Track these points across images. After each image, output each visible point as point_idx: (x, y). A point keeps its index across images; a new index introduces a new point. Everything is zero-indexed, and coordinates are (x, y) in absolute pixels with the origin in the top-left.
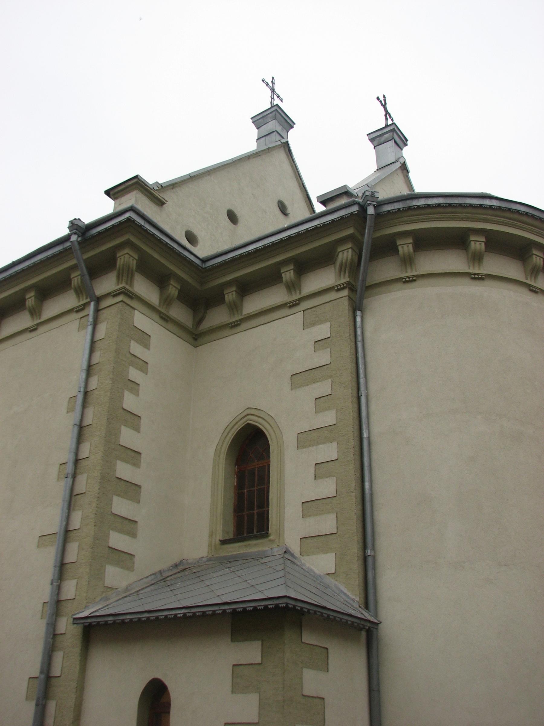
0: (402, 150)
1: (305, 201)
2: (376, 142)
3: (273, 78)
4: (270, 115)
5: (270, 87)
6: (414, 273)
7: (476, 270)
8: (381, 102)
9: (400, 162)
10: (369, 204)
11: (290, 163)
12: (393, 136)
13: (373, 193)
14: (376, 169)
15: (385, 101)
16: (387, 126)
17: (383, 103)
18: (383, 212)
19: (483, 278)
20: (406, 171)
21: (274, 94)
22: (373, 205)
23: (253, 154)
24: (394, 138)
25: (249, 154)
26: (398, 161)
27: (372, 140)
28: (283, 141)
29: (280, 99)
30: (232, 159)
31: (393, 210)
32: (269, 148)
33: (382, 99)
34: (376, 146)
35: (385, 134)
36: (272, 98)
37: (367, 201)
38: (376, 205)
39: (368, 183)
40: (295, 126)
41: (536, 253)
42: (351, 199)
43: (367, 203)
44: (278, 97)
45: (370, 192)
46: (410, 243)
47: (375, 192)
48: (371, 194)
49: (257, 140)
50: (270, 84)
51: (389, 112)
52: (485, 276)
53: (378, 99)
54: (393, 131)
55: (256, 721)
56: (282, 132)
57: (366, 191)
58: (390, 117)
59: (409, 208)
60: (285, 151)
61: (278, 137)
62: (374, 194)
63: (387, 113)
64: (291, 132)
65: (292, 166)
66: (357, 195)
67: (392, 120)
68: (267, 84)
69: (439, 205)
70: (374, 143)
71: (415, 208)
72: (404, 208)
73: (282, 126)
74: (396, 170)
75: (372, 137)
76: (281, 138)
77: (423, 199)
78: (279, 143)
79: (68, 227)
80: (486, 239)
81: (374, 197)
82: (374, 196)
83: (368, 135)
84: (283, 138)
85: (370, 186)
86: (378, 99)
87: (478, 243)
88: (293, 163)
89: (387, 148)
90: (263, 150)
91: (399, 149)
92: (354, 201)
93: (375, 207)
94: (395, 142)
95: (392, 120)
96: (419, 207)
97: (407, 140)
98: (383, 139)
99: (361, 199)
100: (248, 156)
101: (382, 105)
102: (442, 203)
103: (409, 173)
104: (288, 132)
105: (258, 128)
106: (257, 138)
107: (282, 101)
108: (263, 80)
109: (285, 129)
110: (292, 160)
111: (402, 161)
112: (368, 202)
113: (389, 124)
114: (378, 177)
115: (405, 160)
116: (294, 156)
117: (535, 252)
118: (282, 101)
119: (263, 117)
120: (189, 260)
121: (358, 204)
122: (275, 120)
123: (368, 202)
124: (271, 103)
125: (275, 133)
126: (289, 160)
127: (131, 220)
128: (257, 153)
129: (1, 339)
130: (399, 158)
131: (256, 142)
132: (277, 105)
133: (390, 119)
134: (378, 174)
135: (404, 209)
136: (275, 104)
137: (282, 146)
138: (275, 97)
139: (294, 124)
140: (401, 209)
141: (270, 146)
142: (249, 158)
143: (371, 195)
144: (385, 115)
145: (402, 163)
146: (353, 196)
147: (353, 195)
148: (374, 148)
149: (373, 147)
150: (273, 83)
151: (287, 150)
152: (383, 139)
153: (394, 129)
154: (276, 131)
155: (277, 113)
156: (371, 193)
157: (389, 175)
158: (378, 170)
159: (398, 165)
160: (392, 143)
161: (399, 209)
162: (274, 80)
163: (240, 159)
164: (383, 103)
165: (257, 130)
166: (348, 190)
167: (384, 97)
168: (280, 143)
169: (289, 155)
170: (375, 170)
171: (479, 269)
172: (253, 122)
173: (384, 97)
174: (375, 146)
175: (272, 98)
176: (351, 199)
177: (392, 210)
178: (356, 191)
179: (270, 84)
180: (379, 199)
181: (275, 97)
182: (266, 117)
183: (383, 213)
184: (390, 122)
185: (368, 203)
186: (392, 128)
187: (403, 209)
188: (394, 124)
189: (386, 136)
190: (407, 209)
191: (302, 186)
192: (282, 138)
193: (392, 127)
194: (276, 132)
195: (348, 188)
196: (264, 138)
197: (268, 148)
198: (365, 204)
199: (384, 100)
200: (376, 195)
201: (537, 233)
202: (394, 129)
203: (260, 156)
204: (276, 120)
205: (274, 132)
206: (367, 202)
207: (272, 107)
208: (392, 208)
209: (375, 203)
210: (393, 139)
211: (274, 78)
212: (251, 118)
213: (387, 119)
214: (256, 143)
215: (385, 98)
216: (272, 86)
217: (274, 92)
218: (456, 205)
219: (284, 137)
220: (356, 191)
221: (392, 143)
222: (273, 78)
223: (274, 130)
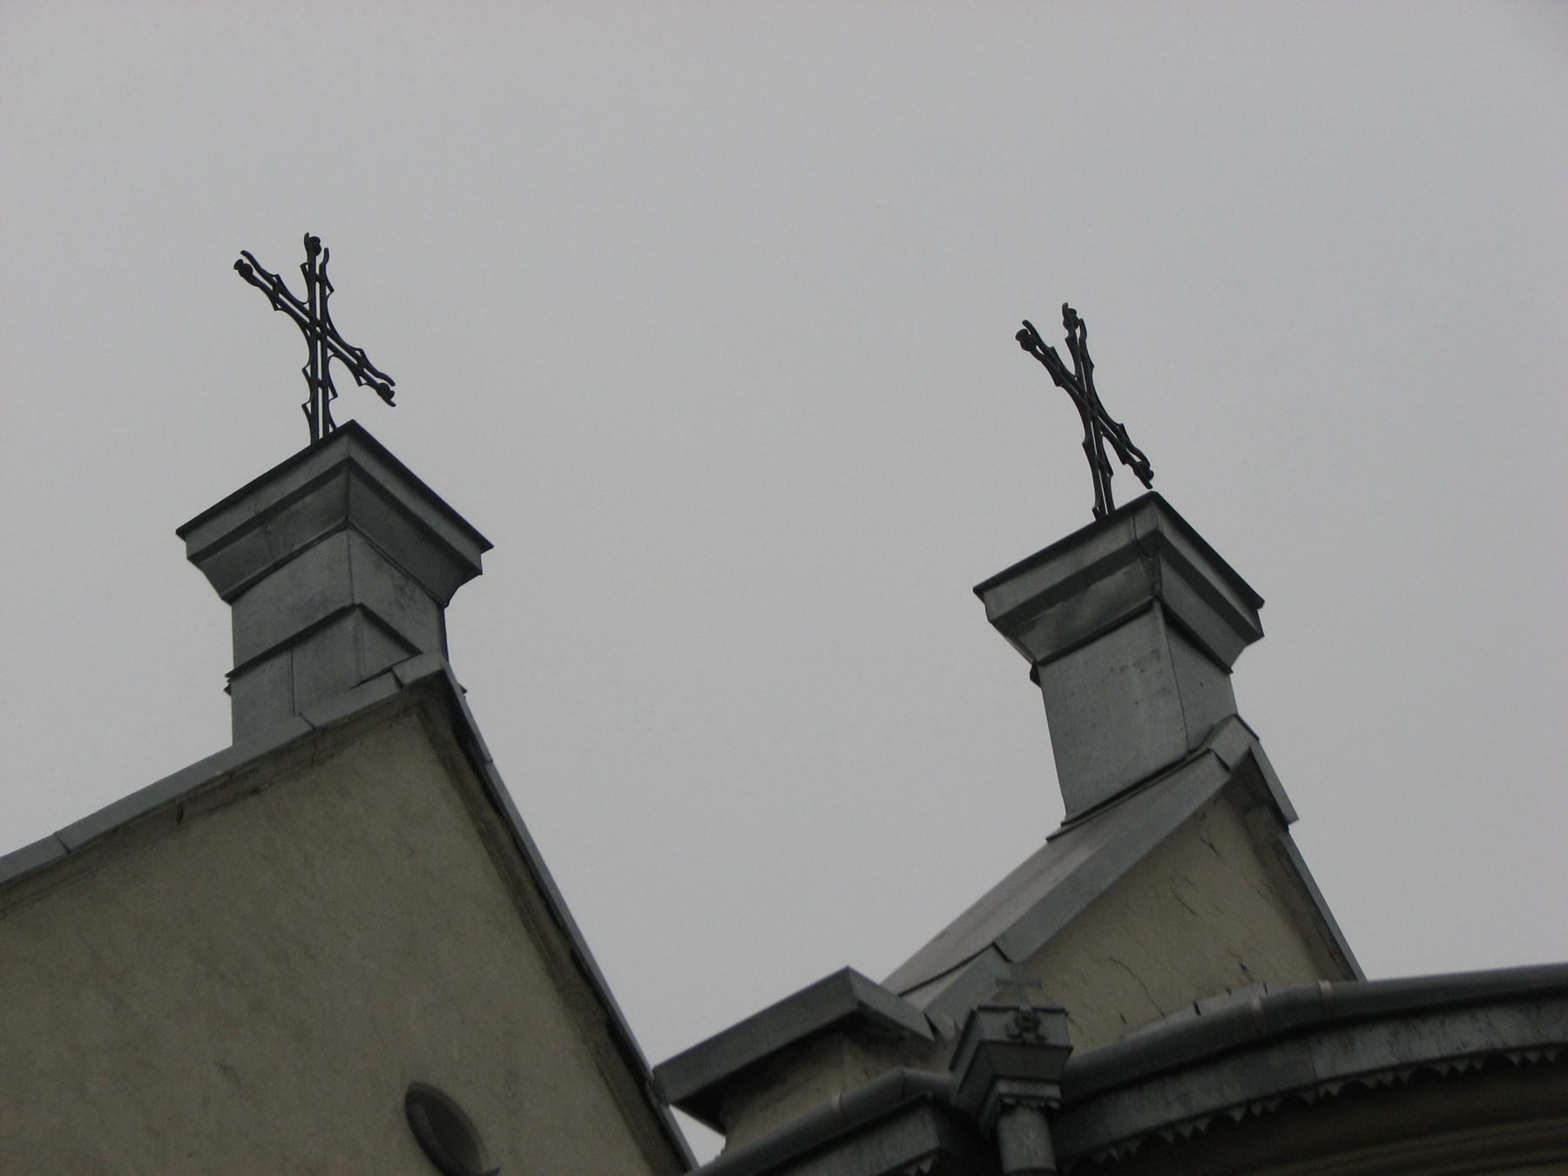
0: (1227, 671)
1: (601, 1073)
2: (1043, 634)
3: (312, 245)
4: (308, 499)
5: (299, 305)
8: (1049, 358)
9: (1217, 756)
10: (1009, 1101)
11: (476, 817)
12: (1153, 585)
13: (1029, 1022)
14: (1061, 815)
15: (1078, 347)
16: (1107, 517)
17: (1070, 365)
18: (1116, 1144)
20: (1266, 815)
21: (330, 353)
22: (1034, 1104)
23: (203, 785)
24: (1159, 597)
25: (181, 789)
26: (1208, 751)
27: (1011, 625)
28: (413, 671)
29: (371, 383)
30: (57, 835)
31: (1182, 1121)
32: (316, 735)
33: (1054, 335)
34: (1046, 662)
35: (1102, 576)
36: (320, 384)
37: (996, 1078)
38: (1055, 1105)
39: (1004, 937)
40: (486, 558)
42: (889, 1073)
43: (992, 1099)
44: (360, 367)
45: (1011, 1014)
47: (1041, 1015)
48: (1015, 1031)
49: (232, 676)
50: (298, 287)
51: (1117, 418)
53: (1029, 339)
54: (1150, 547)
56: (402, 607)
57: (983, 1009)
58: (1126, 449)
59: (1294, 1103)
60: (433, 740)
61: (377, 651)
62: (1037, 1024)
63: (1099, 427)
64: (465, 606)
65: (486, 837)
66: (927, 1033)
67: (1144, 472)
68: (276, 291)
69: (1495, 1063)
70: (1031, 639)
71: (1328, 1094)
72: (1248, 1103)
73: (398, 567)
74: (1200, 816)
75: (1007, 606)
76: (398, 654)
77: (1382, 1033)
78: (384, 690)
81: (1041, 1044)
82: (1041, 1038)
83: (980, 591)
84: (413, 651)
85: (1017, 955)
86: (1029, 339)
88: (490, 814)
89: (1122, 670)
90: (276, 755)
91: (1204, 669)
92: (905, 1085)
93: (1050, 1115)
94: (1175, 625)
95: (1144, 472)
96: (1355, 1088)
97: (1254, 602)
98: (1087, 608)
99: (952, 1067)
100: (172, 801)
101: (1060, 376)
102: (1513, 1043)
103: (1293, 829)
104: (441, 604)
105: (230, 598)
106: (231, 668)
107: (386, 393)
108: (246, 261)
109: (423, 587)
110: (483, 799)
111: (1229, 747)
113: (1119, 501)
114: (1073, 882)
115: (1257, 739)
116: (496, 762)
118: (386, 393)
119: (261, 519)
121: (936, 1103)
122: (341, 538)
123: (1002, 1087)
124: (312, 419)
125: (349, 624)
126: (464, 792)
128: (231, 776)
129: (13, 884)
130: (1212, 732)
131: (228, 690)
132: (353, 429)
133: (1128, 469)
134: (1080, 856)
135: (1257, 1110)
136: (340, 420)
137: (406, 709)
138: (339, 371)
139: (485, 545)
140: (1237, 1115)
141: (320, 719)
142: (180, 818)
143: (1020, 1036)
144: (1087, 446)
145: (1230, 762)
146: (901, 1039)
147: (906, 1034)
148: (1035, 677)
149: (1029, 667)
150: (316, 277)
151: (447, 733)
152: (1087, 608)
153: (1156, 536)
154: (361, 606)
155: (358, 487)
156: (1016, 1021)
157: (1150, 860)
158: (1069, 825)
159: (1206, 780)
160: (1147, 633)
161: (1219, 1118)
162: (319, 259)
163: (114, 831)
164: (1070, 365)
165: (227, 609)
166: (861, 1004)
167: (1071, 319)
168: (394, 690)
169: (463, 763)
170: (1054, 826)
172: (195, 558)
173: (1071, 319)
174: (1039, 658)
175: (313, 383)
176: (889, 1073)
177: (1170, 1125)
178: (921, 1001)
179: (298, 287)
180: (1074, 1055)
181: (339, 371)
182: (286, 513)
183: (1114, 1153)
184: (1126, 488)
185: (1001, 1096)
186: (1140, 534)
187: (1248, 1115)
188: (1154, 500)
189: (1108, 585)
190: (1272, 1107)
191: (572, 969)
192: (406, 656)
193: (1142, 526)
194: (358, 614)
195: (862, 994)
196: (281, 662)
197: (307, 735)
199: (1071, 341)
200: (1052, 1030)
202: (1156, 536)
203: (256, 791)
204: (351, 533)
205: (343, 613)
206: (992, 1085)
207: (317, 447)
208: (1176, 1113)
209: (1053, 1091)
210: (1157, 605)
211: (323, 245)
212: (183, 532)
213: (1101, 470)
214: (227, 700)
215: (1078, 331)
216: (312, 300)
217: (324, 342)
219: (418, 643)
220: (921, 1001)
221: (1147, 633)
222: (312, 245)
223: (347, 603)
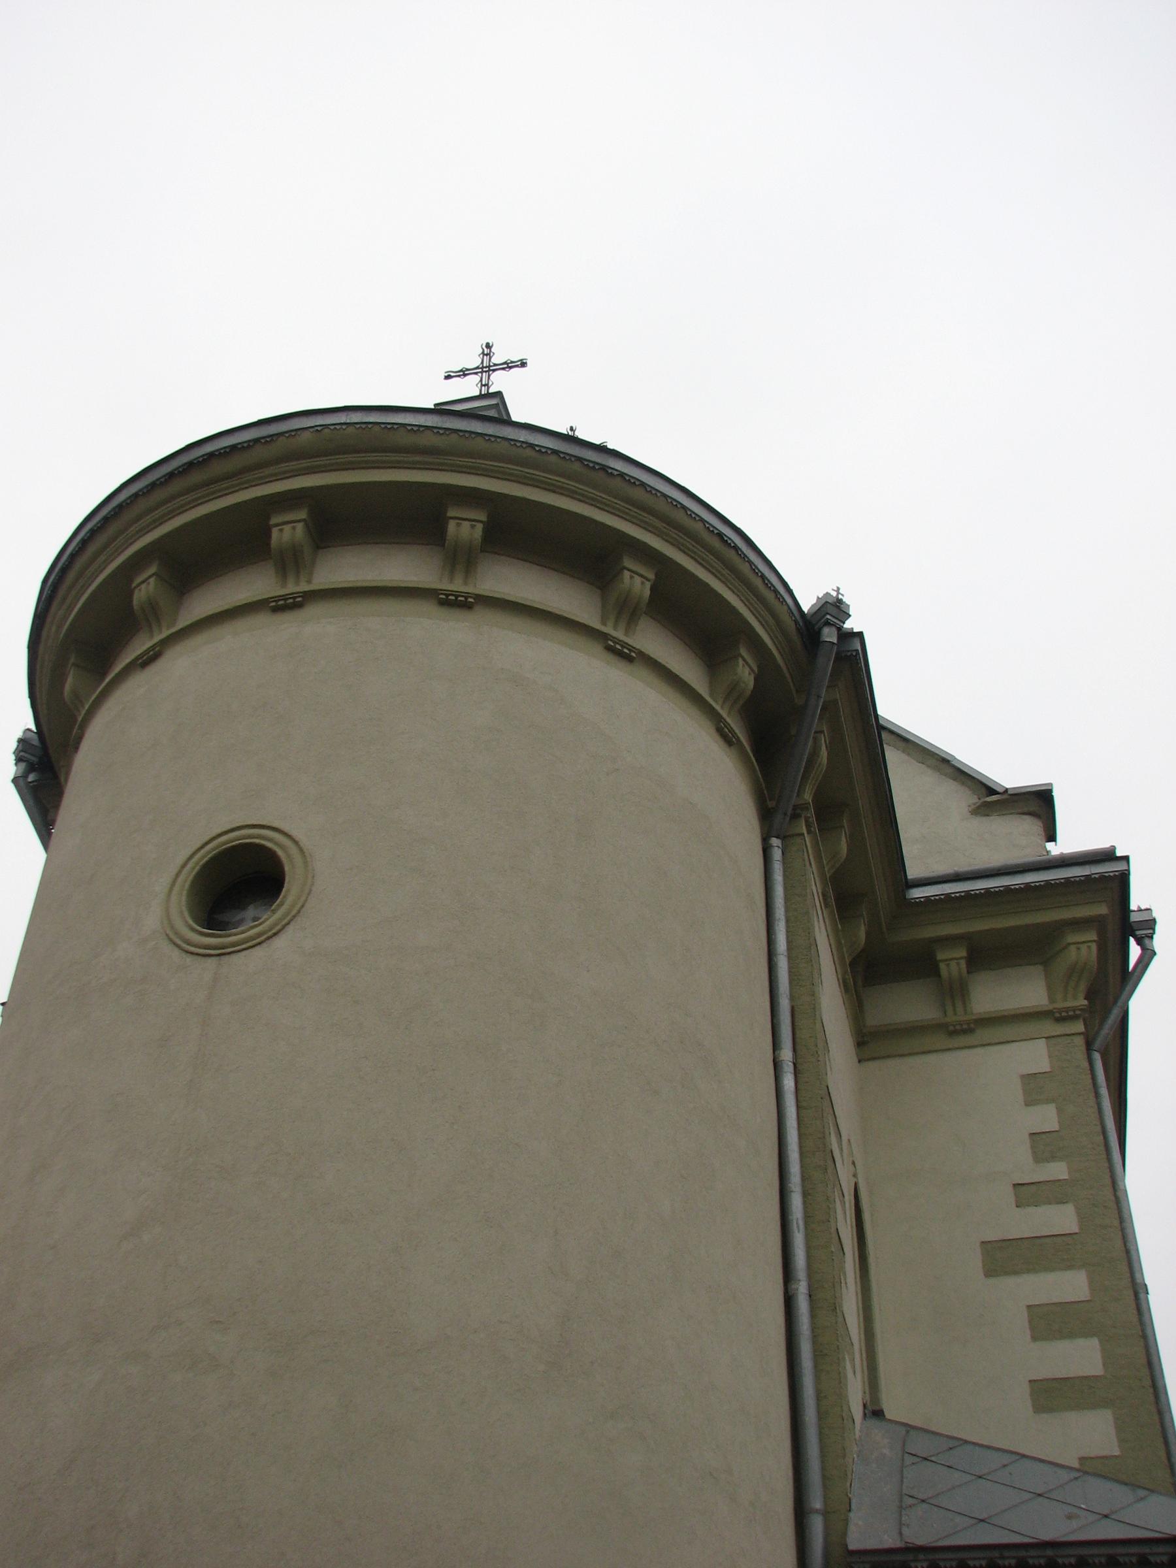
6: (304, 587)
7: (457, 585)
19: (470, 602)
37: (828, 614)
41: (631, 566)
46: (299, 521)
52: (474, 599)
55: (1048, 1070)
79: (12, 777)
80: (656, 575)
87: (466, 524)
112: (828, 617)
117: (628, 562)
120: (917, 900)
123: (828, 617)
127: (941, 898)
171: (466, 583)
198: (820, 620)
201: (619, 510)
218: (634, 483)
